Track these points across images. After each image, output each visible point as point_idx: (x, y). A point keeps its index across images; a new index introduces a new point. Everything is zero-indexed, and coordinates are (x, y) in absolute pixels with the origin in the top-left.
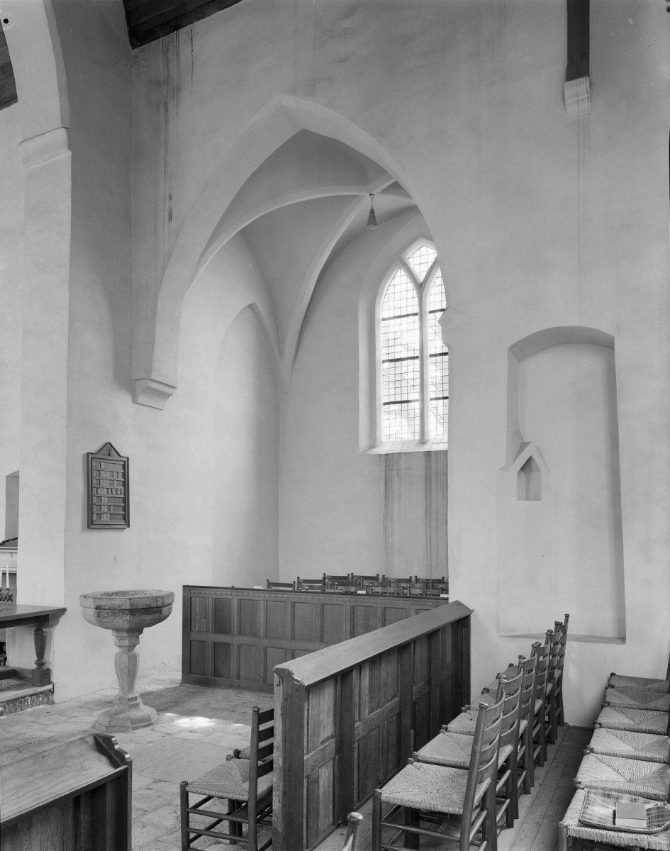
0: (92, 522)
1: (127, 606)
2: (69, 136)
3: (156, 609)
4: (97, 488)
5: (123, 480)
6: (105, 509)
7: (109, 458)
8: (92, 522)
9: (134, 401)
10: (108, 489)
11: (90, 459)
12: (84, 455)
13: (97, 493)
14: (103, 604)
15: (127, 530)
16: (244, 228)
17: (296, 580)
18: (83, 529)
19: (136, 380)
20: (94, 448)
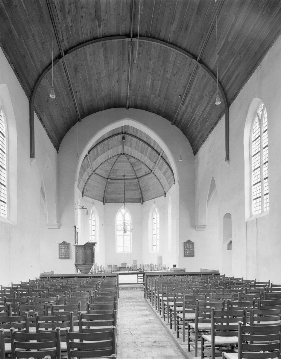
20: (185, 241)
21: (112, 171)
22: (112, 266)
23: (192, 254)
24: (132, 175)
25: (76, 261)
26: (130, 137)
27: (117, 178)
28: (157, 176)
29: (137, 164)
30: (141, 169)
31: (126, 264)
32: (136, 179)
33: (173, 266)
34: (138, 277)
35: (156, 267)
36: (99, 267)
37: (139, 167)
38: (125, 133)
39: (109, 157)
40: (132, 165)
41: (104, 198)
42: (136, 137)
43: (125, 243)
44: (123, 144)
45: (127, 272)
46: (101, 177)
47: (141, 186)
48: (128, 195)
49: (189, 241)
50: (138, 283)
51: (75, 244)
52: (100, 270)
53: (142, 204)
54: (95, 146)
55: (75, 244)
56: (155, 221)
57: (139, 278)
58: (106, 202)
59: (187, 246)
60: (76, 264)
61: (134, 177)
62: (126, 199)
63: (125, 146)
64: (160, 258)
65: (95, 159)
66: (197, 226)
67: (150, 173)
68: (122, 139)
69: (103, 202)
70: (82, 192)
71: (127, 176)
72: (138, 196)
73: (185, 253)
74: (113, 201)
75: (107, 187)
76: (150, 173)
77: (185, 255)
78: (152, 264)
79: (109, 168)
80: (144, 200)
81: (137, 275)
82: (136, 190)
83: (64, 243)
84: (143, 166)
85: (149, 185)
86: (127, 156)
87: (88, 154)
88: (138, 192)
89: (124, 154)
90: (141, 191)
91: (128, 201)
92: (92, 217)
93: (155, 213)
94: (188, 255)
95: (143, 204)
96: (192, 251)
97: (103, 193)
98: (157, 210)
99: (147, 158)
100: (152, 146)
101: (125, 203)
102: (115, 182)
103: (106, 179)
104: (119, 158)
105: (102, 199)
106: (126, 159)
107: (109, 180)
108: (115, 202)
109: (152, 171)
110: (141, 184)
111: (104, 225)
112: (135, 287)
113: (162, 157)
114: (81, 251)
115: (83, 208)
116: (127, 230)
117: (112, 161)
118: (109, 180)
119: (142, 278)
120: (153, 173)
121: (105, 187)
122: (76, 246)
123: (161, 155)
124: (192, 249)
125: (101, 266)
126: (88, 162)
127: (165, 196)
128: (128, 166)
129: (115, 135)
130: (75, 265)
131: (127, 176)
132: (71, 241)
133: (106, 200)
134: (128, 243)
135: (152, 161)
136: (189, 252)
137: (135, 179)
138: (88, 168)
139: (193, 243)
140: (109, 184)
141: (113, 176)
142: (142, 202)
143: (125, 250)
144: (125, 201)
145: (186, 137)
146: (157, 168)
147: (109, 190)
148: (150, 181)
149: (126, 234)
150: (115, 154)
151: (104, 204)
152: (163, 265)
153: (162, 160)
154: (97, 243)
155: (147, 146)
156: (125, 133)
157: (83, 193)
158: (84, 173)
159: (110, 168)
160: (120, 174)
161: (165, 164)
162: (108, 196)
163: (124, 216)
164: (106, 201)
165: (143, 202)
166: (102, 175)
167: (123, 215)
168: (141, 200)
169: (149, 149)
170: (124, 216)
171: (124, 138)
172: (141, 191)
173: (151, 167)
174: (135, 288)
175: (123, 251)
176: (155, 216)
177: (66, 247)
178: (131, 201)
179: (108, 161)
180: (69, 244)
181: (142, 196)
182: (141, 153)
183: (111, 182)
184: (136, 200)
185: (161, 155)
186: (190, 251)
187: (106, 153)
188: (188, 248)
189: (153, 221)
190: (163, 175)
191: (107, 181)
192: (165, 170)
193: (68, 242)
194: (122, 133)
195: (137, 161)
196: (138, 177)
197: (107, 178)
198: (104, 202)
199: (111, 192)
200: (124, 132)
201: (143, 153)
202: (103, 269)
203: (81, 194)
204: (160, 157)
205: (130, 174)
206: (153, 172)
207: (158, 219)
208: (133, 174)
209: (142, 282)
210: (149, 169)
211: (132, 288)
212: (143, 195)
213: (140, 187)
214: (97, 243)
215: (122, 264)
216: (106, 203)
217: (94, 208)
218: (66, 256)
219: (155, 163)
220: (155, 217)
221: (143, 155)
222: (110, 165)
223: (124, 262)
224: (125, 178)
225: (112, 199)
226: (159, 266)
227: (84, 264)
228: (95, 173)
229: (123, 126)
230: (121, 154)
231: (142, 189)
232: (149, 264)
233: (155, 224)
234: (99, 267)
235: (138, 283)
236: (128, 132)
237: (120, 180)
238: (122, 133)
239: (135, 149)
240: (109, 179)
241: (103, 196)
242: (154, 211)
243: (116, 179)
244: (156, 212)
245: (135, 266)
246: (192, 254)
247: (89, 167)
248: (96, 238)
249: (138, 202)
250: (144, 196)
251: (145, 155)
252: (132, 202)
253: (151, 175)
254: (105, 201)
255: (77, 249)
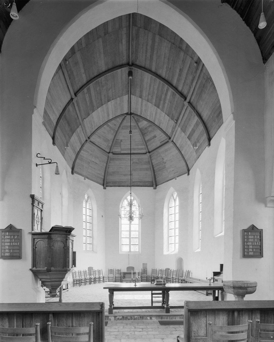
0: (245, 255)
1: (232, 286)
2: (234, 116)
3: (244, 288)
4: (247, 243)
5: (260, 238)
6: (251, 250)
7: (253, 230)
8: (245, 255)
9: (266, 206)
10: (252, 242)
11: (245, 232)
12: (241, 230)
13: (247, 244)
14: (225, 284)
15: (262, 258)
16: (119, 224)
17: (87, 270)
18: (241, 258)
19: (267, 198)
20: (246, 227)
21: (115, 142)
22: (115, 270)
23: (259, 253)
24: (142, 148)
25: (34, 263)
26: (140, 71)
27: (122, 152)
28: (178, 146)
29: (150, 129)
30: (155, 137)
31: (133, 268)
32: (148, 154)
33: (213, 274)
34: (152, 294)
35: (175, 274)
36: (97, 272)
37: (152, 135)
38: (133, 64)
39: (111, 117)
40: (143, 132)
41: (104, 181)
42: (149, 71)
43: (131, 240)
44: (130, 93)
45: (132, 285)
46: (99, 148)
47: (153, 164)
48: (137, 176)
49: (253, 228)
50: (152, 307)
51: (33, 230)
52: (97, 276)
53: (155, 188)
54: (85, 84)
55: (33, 230)
56: (172, 211)
57: (153, 296)
58: (107, 186)
59: (250, 237)
60: (34, 269)
61: (144, 151)
62: (134, 182)
63: (133, 97)
64: (180, 261)
65: (89, 115)
66: (269, 199)
67: (168, 142)
68: (127, 76)
69: (103, 185)
70: (71, 166)
71: (134, 149)
72: (149, 178)
73: (246, 250)
74: (117, 185)
75: (109, 166)
76: (168, 142)
77: (246, 253)
78: (169, 269)
79: (110, 137)
80: (158, 184)
81: (150, 292)
82: (147, 169)
83: (11, 228)
84: (158, 133)
85: (164, 161)
86: (136, 117)
87: (74, 96)
88: (150, 173)
89: (131, 114)
90: (154, 170)
91: (136, 185)
92: (88, 204)
93: (173, 200)
94: (251, 254)
95: (156, 189)
96: (259, 247)
97: (103, 174)
98: (175, 195)
99: (164, 114)
100: (174, 84)
101: (132, 187)
102: (119, 157)
103: (108, 154)
104: (125, 121)
105: (102, 182)
106: (133, 124)
107: (111, 154)
108: (119, 186)
109: (170, 138)
110: (153, 161)
111: (103, 217)
112: (148, 316)
113: (189, 102)
114: (42, 244)
115: (50, 163)
116: (134, 216)
117: (115, 125)
118: (111, 154)
119: (161, 295)
120: (172, 141)
121: (105, 165)
122: (33, 234)
123: (188, 100)
124: (258, 243)
125: (99, 271)
126: (76, 116)
127: (189, 174)
128: (137, 135)
129: (117, 67)
130: (31, 273)
131: (134, 149)
132: (23, 224)
133: (107, 183)
134: (136, 241)
135: (172, 119)
136: (253, 249)
137: (146, 153)
138: (78, 127)
139: (261, 232)
140: (111, 161)
141: (116, 150)
142: (154, 186)
143: (131, 251)
144: (132, 185)
145: (248, 28)
146: (179, 129)
147: (111, 170)
148: (169, 154)
149: (132, 223)
150: (119, 113)
151: (105, 188)
152: (185, 271)
153: (189, 108)
154: (73, 229)
155: (166, 86)
156: (133, 64)
157: (73, 169)
158: (73, 134)
159: (112, 137)
160: (125, 147)
161: (194, 114)
162: (110, 178)
163: (131, 205)
164: (107, 185)
165: (156, 186)
166: (100, 147)
167: (130, 202)
168: (154, 183)
169: (171, 90)
170: (131, 205)
171: (130, 73)
172: (154, 170)
173: (169, 132)
174: (149, 318)
175: (129, 250)
176: (172, 204)
177: (14, 236)
178: (141, 184)
179: (109, 124)
180: (19, 231)
181: (155, 177)
182: (156, 107)
183: (114, 159)
184: (147, 184)
185: (188, 100)
186: (254, 247)
187: (104, 106)
188: (251, 240)
189: (170, 210)
190: (188, 139)
191: (108, 157)
192: (193, 129)
193: (18, 227)
194: (128, 64)
195: (150, 124)
196: (150, 150)
197: (108, 151)
198: (105, 185)
199: (114, 172)
200: (130, 63)
201: (158, 107)
202: (101, 276)
203: (51, 140)
204: (186, 103)
205: (140, 147)
206: (172, 139)
207: (177, 208)
208: (144, 147)
209: (160, 305)
210: (167, 135)
211: (142, 317)
212: (156, 177)
213: (153, 166)
214: (73, 229)
215: (128, 268)
216: (107, 188)
217: (90, 192)
218: (15, 254)
219: (177, 120)
220: (173, 205)
221: (159, 110)
222: (112, 132)
223: (130, 266)
224: (133, 152)
225: (115, 182)
226: (178, 272)
227: (49, 271)
228: (90, 141)
229: (130, 14)
230: (127, 114)
231: (155, 169)
232: (164, 269)
233: (173, 215)
234: (97, 272)
235: (152, 307)
236: (137, 63)
237: (126, 155)
238: (128, 64)
239: (148, 101)
240: (111, 153)
241: (103, 177)
242: (172, 197)
243: (119, 153)
244: (175, 198)
245: (145, 271)
246: (259, 253)
247: (80, 126)
248: (92, 232)
249: (149, 186)
250: (158, 177)
251: (162, 110)
252: (141, 186)
253: (170, 145)
254: (105, 184)
255: (36, 240)
